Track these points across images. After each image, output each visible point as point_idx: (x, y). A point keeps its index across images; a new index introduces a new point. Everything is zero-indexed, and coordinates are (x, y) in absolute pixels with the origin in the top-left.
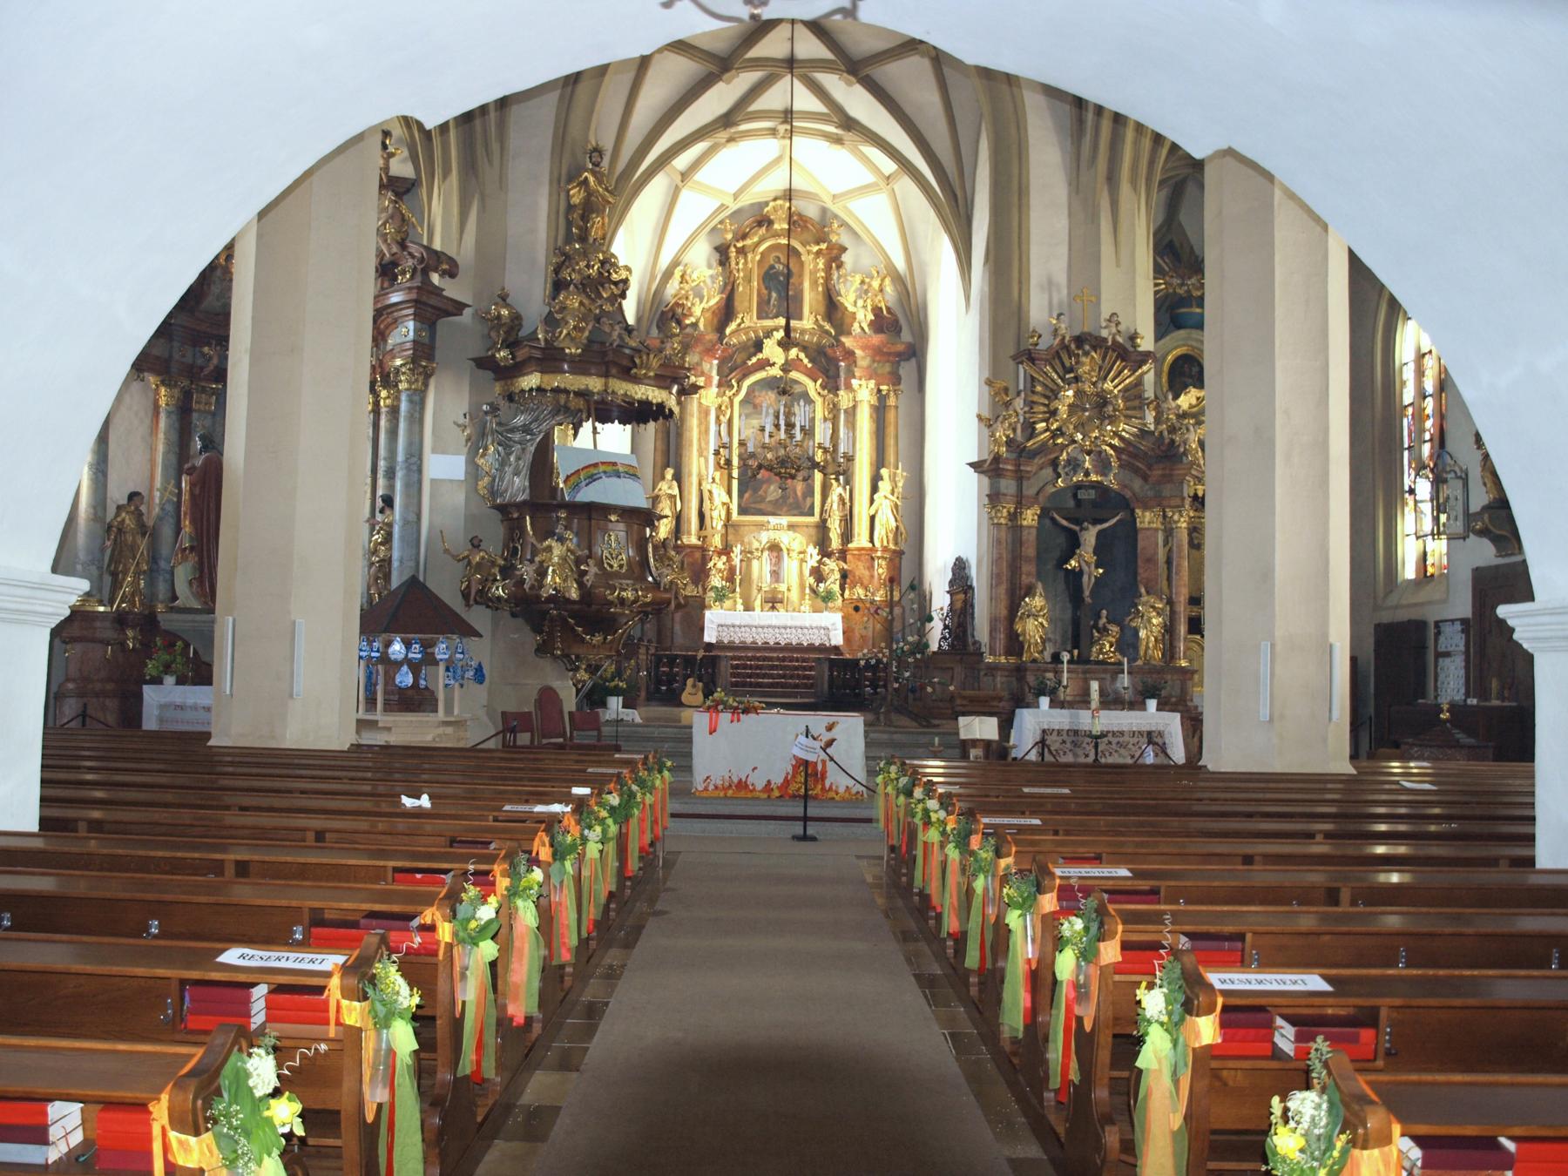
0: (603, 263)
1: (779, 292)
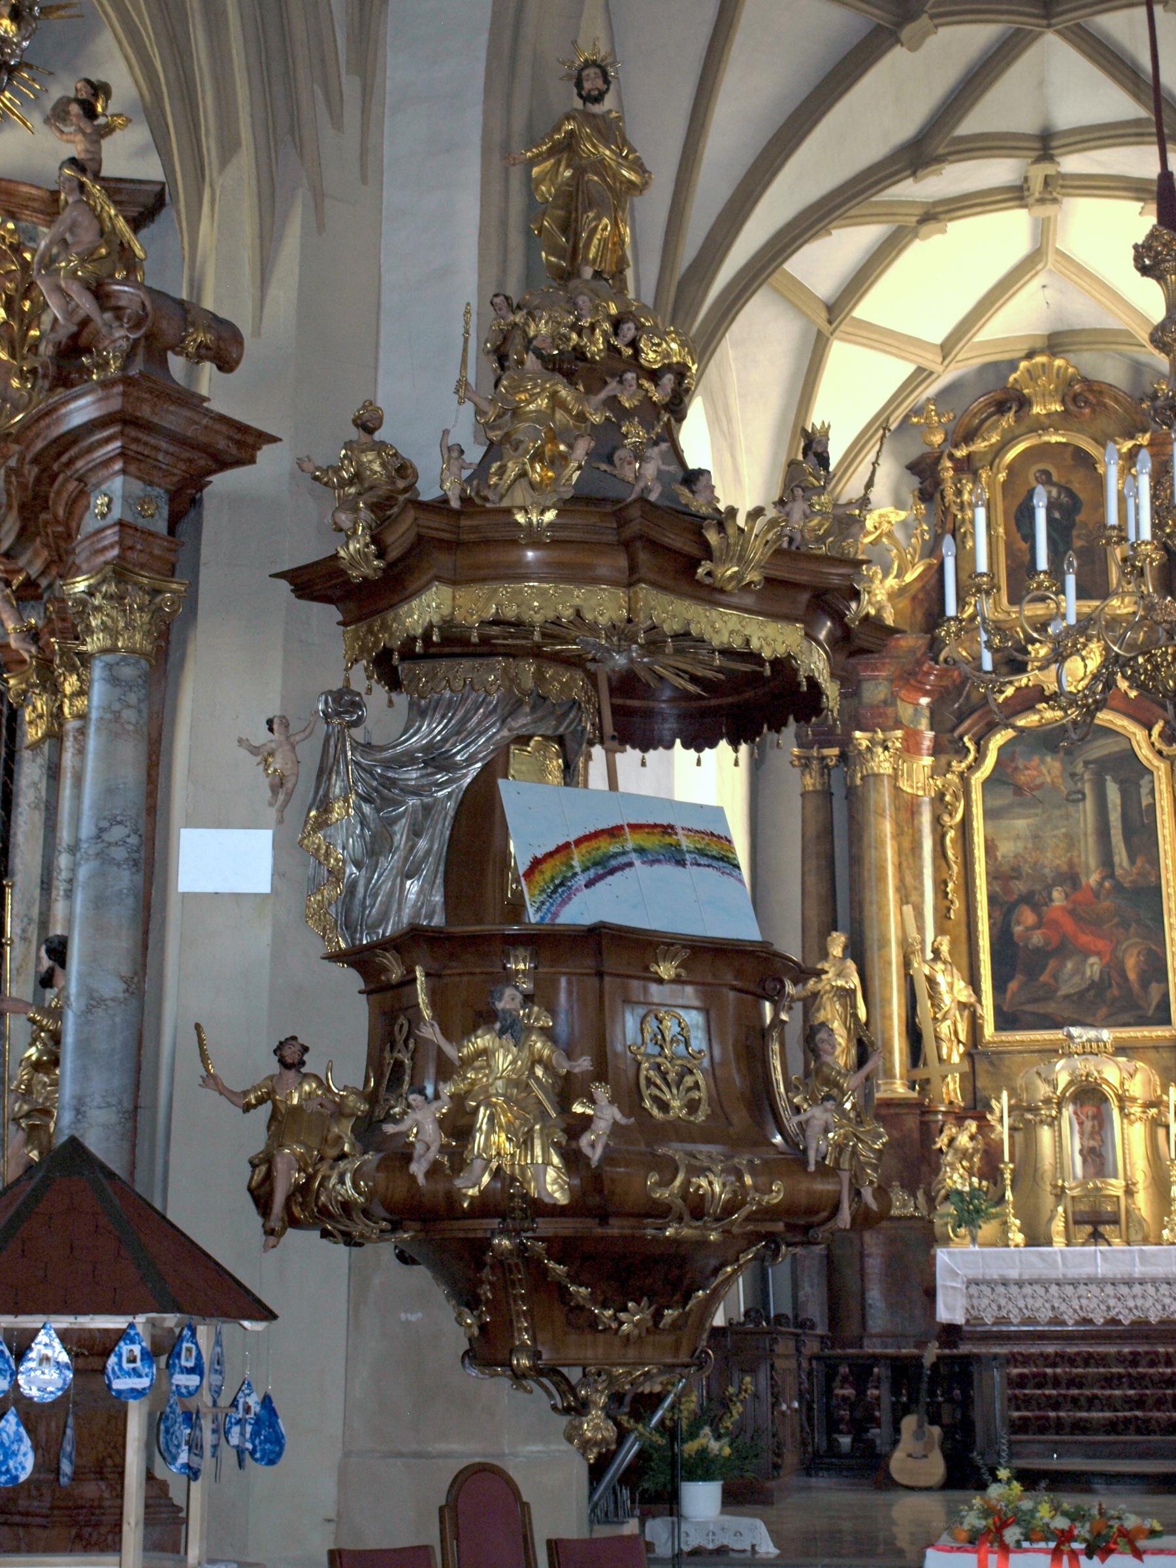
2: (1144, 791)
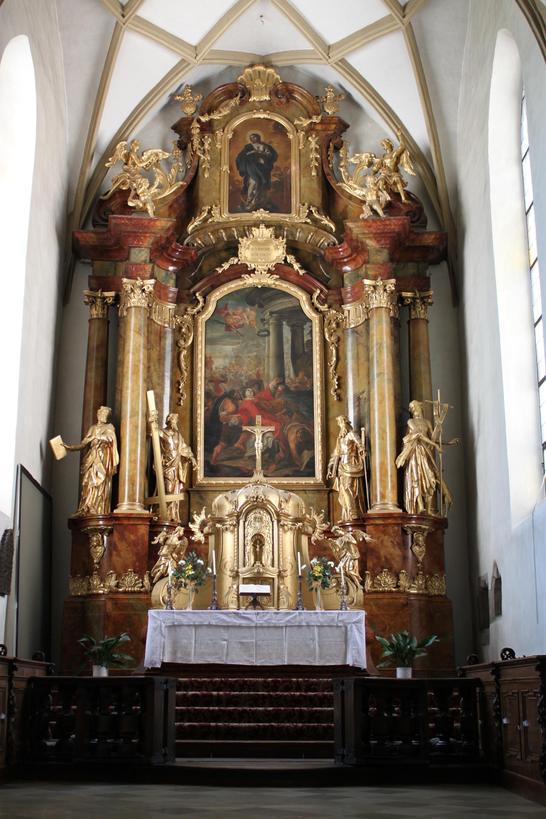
1: (259, 179)
2: (306, 332)
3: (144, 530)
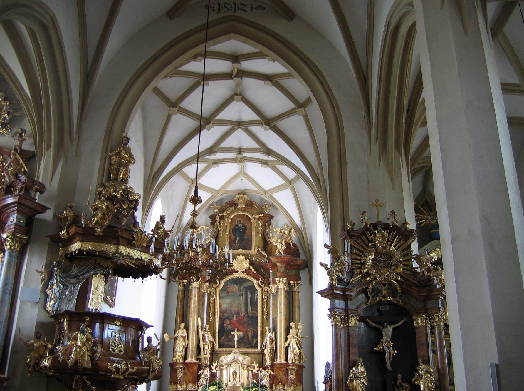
0: (124, 191)
2: (256, 295)
3: (196, 368)
